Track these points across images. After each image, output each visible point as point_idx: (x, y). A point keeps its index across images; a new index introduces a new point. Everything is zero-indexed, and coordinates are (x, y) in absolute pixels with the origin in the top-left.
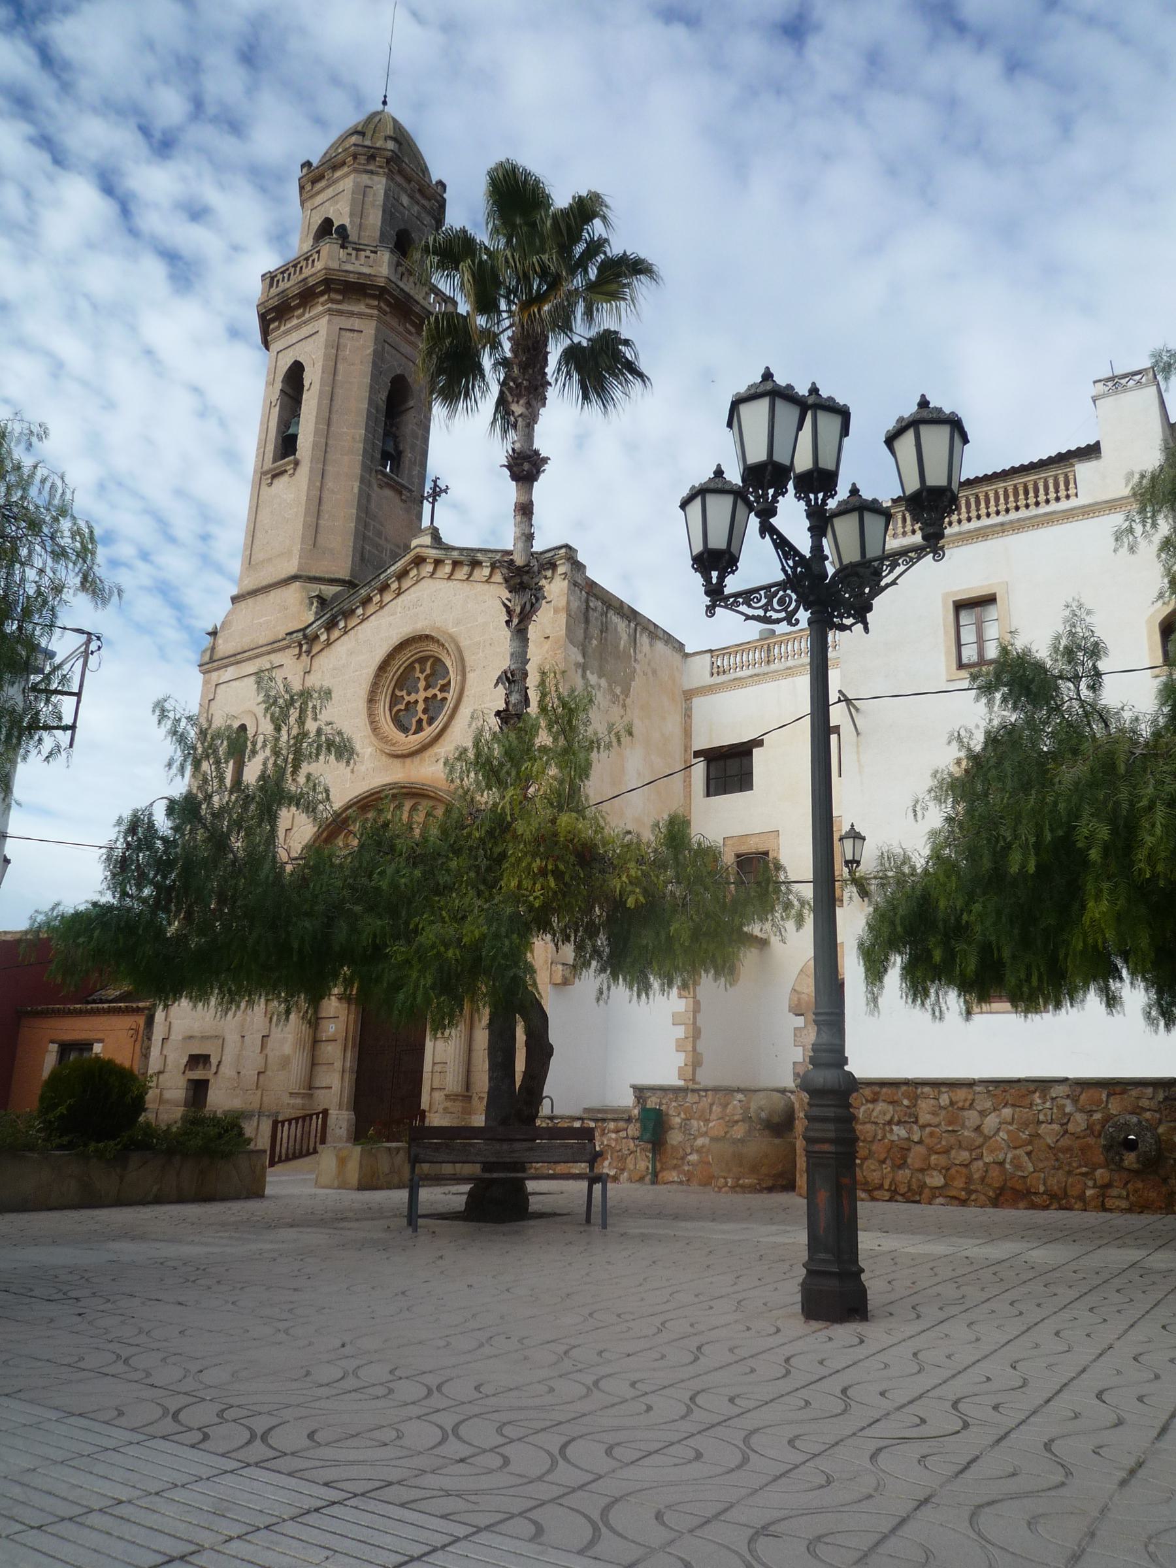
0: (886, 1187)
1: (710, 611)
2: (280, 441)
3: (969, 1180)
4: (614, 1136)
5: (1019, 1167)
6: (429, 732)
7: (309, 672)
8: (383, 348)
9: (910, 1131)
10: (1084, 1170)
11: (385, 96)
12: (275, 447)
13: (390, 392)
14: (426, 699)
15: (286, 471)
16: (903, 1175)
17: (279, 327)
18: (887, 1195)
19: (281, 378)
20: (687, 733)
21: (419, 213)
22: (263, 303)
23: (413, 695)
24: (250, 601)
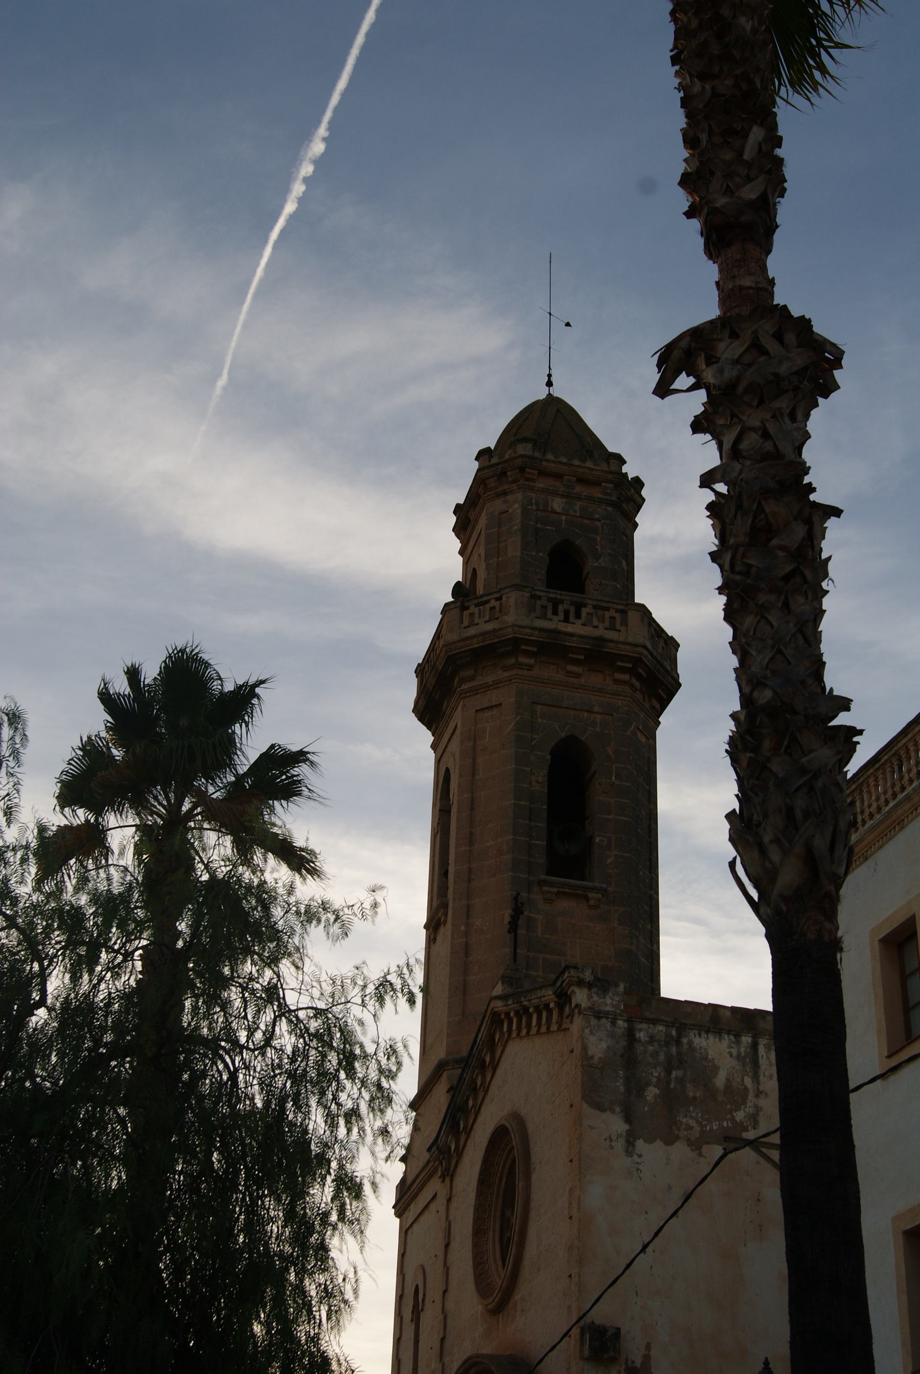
11: (549, 376)
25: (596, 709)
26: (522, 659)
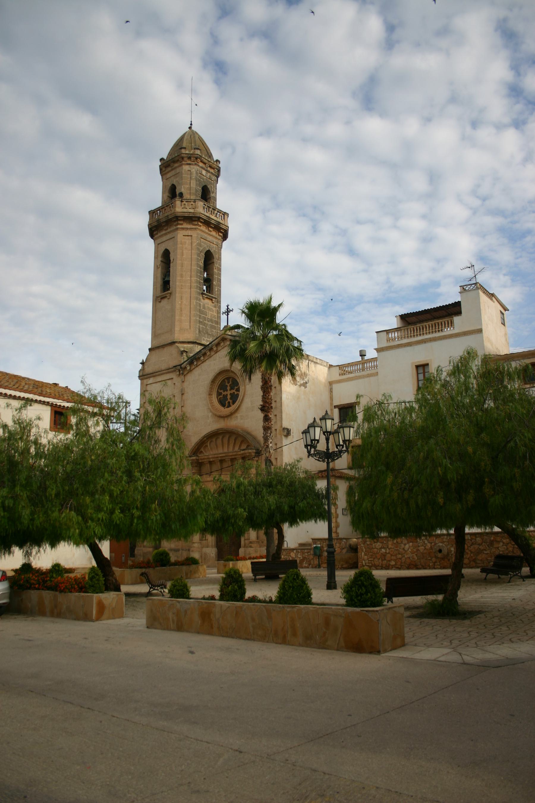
0: (380, 565)
1: (308, 457)
2: (162, 283)
3: (401, 563)
4: (306, 554)
5: (414, 558)
6: (233, 407)
7: (183, 382)
8: (201, 241)
9: (386, 550)
10: (430, 558)
11: (191, 122)
12: (161, 286)
13: (205, 258)
14: (231, 394)
15: (166, 297)
16: (385, 562)
17: (157, 234)
18: (380, 568)
19: (161, 256)
20: (331, 398)
21: (210, 176)
22: (150, 224)
23: (225, 392)
24: (157, 351)
25: (214, 243)
26: (199, 223)
